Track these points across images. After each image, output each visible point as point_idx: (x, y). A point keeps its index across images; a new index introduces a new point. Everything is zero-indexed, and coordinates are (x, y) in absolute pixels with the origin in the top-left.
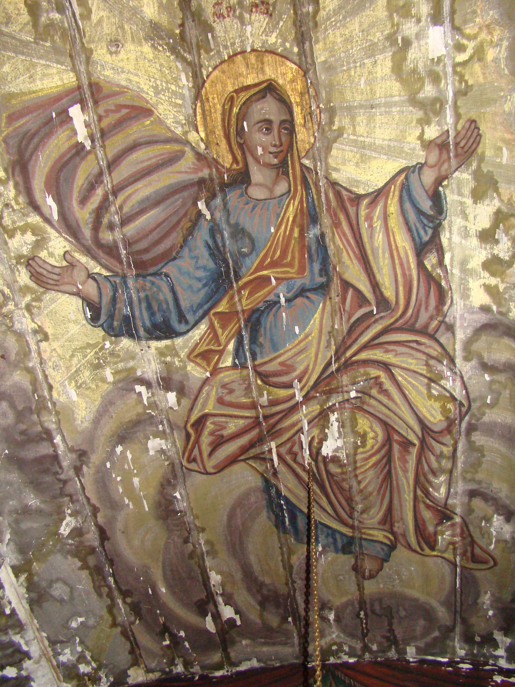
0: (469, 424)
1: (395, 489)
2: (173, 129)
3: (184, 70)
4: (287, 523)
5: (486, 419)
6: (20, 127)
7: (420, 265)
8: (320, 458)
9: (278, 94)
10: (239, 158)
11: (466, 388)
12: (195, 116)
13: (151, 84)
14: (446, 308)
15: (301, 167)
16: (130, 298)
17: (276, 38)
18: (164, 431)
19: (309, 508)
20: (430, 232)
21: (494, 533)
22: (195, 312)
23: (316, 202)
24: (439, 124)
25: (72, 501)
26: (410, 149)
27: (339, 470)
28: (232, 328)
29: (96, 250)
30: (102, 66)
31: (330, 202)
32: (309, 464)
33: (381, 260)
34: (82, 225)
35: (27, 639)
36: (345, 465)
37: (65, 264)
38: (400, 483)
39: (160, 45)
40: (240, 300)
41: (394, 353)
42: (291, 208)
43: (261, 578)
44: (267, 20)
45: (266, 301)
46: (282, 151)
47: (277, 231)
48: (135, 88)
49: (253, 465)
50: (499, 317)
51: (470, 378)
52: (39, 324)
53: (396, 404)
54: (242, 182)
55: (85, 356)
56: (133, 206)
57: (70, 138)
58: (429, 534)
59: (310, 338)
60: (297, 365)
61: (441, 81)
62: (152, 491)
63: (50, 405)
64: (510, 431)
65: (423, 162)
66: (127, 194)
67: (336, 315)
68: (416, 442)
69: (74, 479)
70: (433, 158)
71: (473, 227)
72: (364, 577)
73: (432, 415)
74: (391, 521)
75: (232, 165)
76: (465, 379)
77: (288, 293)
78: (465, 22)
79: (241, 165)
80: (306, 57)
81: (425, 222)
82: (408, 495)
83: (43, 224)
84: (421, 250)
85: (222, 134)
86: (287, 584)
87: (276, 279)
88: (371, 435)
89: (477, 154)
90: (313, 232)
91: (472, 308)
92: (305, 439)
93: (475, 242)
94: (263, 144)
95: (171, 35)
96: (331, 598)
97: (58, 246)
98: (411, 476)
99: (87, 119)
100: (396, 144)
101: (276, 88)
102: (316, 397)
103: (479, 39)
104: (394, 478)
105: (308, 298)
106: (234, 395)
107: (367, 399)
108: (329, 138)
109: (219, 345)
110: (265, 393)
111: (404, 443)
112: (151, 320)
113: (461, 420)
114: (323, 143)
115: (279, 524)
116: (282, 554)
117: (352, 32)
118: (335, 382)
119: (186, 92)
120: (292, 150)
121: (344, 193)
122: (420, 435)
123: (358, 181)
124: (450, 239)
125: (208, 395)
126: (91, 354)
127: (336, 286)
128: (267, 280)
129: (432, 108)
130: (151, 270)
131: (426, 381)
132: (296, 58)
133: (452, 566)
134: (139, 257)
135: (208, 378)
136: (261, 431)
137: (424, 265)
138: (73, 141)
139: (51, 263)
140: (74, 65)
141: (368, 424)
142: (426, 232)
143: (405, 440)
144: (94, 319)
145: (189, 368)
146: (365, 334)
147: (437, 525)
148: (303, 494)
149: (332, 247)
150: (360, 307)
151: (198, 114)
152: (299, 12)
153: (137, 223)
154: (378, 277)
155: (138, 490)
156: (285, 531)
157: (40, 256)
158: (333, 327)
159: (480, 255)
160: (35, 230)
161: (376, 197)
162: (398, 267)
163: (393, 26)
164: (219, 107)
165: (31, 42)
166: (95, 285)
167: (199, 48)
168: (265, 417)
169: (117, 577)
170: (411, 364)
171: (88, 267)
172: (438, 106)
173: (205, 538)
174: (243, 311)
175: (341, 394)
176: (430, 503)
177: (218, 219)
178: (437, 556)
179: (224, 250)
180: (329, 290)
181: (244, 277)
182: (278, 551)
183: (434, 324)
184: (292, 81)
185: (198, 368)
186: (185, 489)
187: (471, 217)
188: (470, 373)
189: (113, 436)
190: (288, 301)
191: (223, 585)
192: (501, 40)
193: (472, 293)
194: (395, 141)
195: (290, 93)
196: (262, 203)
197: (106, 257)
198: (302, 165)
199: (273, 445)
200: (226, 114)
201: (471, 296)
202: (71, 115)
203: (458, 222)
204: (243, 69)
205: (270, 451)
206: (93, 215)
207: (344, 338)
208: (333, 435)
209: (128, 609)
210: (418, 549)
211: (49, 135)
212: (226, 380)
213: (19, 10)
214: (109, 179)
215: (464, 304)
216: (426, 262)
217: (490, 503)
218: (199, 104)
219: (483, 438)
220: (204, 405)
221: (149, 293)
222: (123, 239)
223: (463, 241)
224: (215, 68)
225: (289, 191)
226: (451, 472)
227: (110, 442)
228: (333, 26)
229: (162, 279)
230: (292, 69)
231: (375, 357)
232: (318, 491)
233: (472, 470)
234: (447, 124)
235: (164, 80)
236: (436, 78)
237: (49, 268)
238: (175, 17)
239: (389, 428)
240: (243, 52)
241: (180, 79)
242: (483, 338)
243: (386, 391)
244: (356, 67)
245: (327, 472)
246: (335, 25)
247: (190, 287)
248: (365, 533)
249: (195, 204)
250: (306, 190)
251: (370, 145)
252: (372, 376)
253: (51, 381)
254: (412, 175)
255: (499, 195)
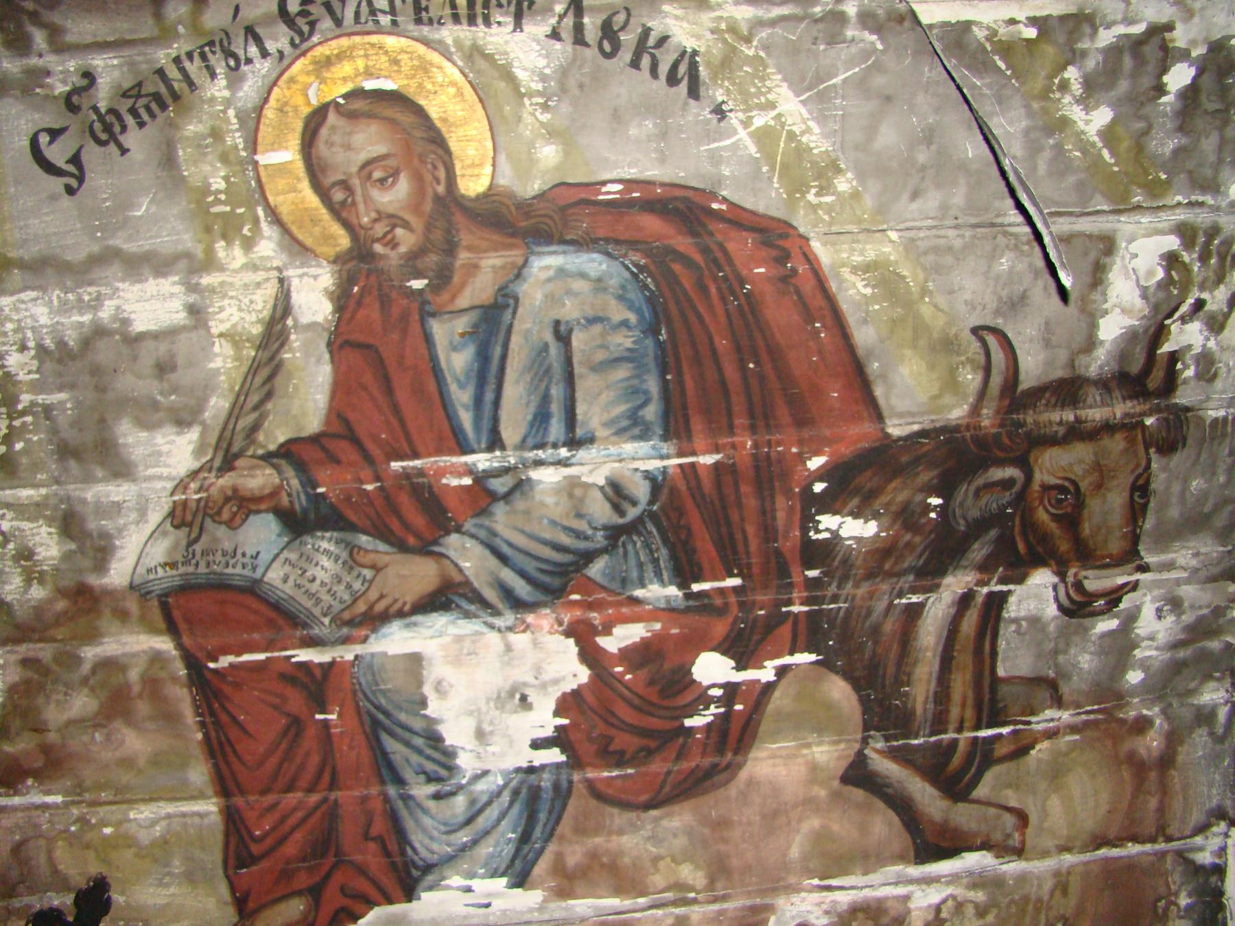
35: (1119, 17)
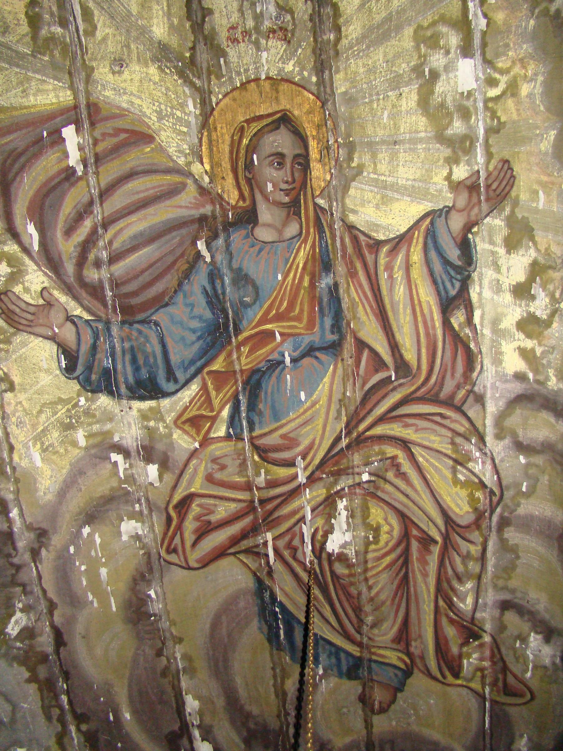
0: (501, 517)
1: (413, 598)
2: (175, 158)
3: (191, 96)
4: (282, 637)
5: (521, 511)
6: (6, 144)
7: (446, 324)
8: (324, 555)
9: (293, 126)
10: (246, 194)
11: (497, 473)
12: (201, 146)
13: (154, 108)
14: (475, 374)
15: (315, 208)
16: (113, 348)
17: (294, 65)
18: (141, 512)
19: (307, 617)
20: (457, 285)
21: (531, 657)
22: (186, 369)
23: (330, 247)
24: (468, 163)
25: (25, 592)
26: (436, 191)
27: (346, 572)
28: (228, 390)
29: (78, 289)
30: (103, 85)
31: (346, 247)
32: (311, 562)
33: (401, 316)
34: (64, 258)
36: (353, 565)
37: (41, 302)
38: (419, 590)
39: (168, 68)
40: (239, 358)
41: (414, 428)
42: (302, 253)
43: (247, 708)
44: (284, 46)
45: (269, 361)
46: (294, 189)
47: (284, 279)
48: (137, 112)
49: (245, 560)
50: (536, 386)
51: (502, 461)
52: (6, 370)
53: (416, 491)
54: (248, 222)
55: (55, 413)
56: (125, 241)
57: (60, 161)
58: (453, 656)
59: (317, 406)
60: (300, 439)
61: (471, 117)
62: (123, 586)
63: (8, 470)
64: (549, 526)
65: (451, 205)
66: (118, 228)
67: (348, 380)
68: (439, 538)
69: (29, 564)
70: (462, 201)
71: (506, 280)
72: (373, 711)
73: (458, 505)
74: (407, 640)
75: (238, 201)
76: (497, 461)
77: (294, 351)
78: (497, 55)
79: (248, 203)
80: (325, 87)
81: (452, 273)
82: (428, 606)
83: (20, 255)
84: (447, 306)
85: (229, 167)
86: (279, 716)
87: (281, 334)
88: (386, 528)
89: (511, 198)
90: (326, 282)
91: (505, 375)
92: (307, 531)
93: (508, 297)
94: (273, 180)
95: (181, 58)
96: (331, 737)
97: (36, 281)
98: (432, 580)
99: (81, 141)
100: (420, 184)
101: (290, 119)
102: (322, 479)
103: (512, 73)
104: (412, 583)
105: (316, 358)
106: (226, 472)
107: (381, 483)
108: (347, 176)
109: (212, 410)
110: (263, 471)
111: (423, 539)
112: (134, 376)
113: (492, 512)
114: (340, 181)
115: (272, 636)
116: (275, 677)
117: (375, 62)
118: (345, 461)
119: (192, 119)
120: (306, 188)
121: (362, 238)
122: (443, 529)
123: (378, 226)
124: (480, 294)
125: (195, 470)
126: (62, 411)
127: (349, 346)
128: (271, 335)
129: (461, 147)
130: (140, 317)
131: (451, 463)
132: (314, 89)
133: (480, 700)
134: (127, 301)
135: (196, 450)
136: (256, 519)
137: (450, 323)
138: (63, 165)
139: (25, 299)
140: (72, 84)
141: (382, 514)
142: (453, 285)
143: (425, 536)
144: (70, 370)
145: (175, 436)
146: (381, 404)
147: (462, 645)
148: (302, 600)
149: (346, 299)
150: (377, 371)
151: (204, 144)
152: (320, 39)
153: (127, 261)
154: (398, 337)
155: (105, 584)
156: (279, 648)
157: (14, 290)
158: (344, 394)
159: (514, 314)
160: (11, 260)
161: (398, 243)
162: (421, 325)
163: (420, 57)
164: (227, 138)
165: (28, 54)
166: (74, 329)
167: (209, 73)
168: (262, 502)
169: (72, 695)
170: (434, 442)
171: (68, 308)
172: (468, 144)
173: (183, 651)
174: (242, 371)
175: (351, 476)
176: (454, 617)
177: (219, 263)
178: (462, 686)
179: (224, 298)
180: (342, 350)
181: (245, 330)
182: (270, 673)
183: (461, 393)
184: (309, 112)
185: (186, 437)
186: (162, 587)
187: (504, 269)
188: (503, 454)
189: (80, 513)
190: (294, 361)
191: (201, 713)
192: (536, 75)
193: (506, 358)
194: (420, 181)
195: (306, 125)
196: (269, 246)
197: (89, 298)
198: (315, 205)
199: (269, 536)
200: (235, 146)
201: (504, 361)
202: (64, 136)
203: (489, 274)
204: (256, 96)
205: (265, 544)
206: (79, 249)
207: (357, 408)
208: (341, 528)
209: (82, 740)
210: (439, 676)
211: (36, 156)
212: (218, 453)
213: (18, 20)
214: (99, 210)
215: (496, 371)
216: (453, 320)
217: (526, 617)
218: (206, 134)
219: (517, 534)
220: (190, 483)
221: (135, 344)
222: (111, 280)
223: (495, 297)
224: (225, 96)
225: (300, 234)
226: (479, 578)
227: (75, 520)
228: (355, 55)
229: (151, 328)
230: (308, 99)
231: (392, 433)
232: (320, 597)
233: (505, 575)
234: (477, 164)
235: (169, 104)
236: (465, 114)
237: (23, 305)
238: (186, 39)
239: (406, 520)
240: (257, 80)
241: (187, 106)
242: (518, 411)
243: (404, 474)
244: (379, 100)
245: (332, 572)
246: (358, 54)
247: (183, 339)
248: (374, 654)
249: (194, 244)
250: (319, 233)
251: (392, 186)
252: (389, 455)
253: (13, 441)
254: (438, 219)
255: (535, 244)
